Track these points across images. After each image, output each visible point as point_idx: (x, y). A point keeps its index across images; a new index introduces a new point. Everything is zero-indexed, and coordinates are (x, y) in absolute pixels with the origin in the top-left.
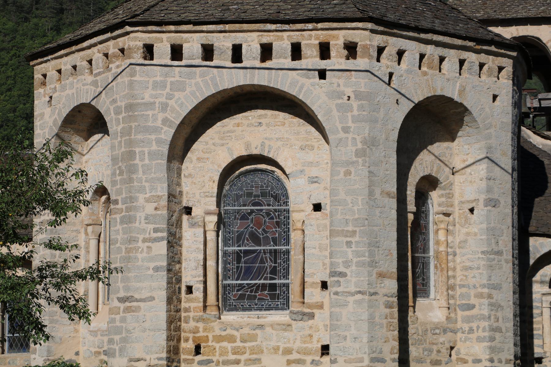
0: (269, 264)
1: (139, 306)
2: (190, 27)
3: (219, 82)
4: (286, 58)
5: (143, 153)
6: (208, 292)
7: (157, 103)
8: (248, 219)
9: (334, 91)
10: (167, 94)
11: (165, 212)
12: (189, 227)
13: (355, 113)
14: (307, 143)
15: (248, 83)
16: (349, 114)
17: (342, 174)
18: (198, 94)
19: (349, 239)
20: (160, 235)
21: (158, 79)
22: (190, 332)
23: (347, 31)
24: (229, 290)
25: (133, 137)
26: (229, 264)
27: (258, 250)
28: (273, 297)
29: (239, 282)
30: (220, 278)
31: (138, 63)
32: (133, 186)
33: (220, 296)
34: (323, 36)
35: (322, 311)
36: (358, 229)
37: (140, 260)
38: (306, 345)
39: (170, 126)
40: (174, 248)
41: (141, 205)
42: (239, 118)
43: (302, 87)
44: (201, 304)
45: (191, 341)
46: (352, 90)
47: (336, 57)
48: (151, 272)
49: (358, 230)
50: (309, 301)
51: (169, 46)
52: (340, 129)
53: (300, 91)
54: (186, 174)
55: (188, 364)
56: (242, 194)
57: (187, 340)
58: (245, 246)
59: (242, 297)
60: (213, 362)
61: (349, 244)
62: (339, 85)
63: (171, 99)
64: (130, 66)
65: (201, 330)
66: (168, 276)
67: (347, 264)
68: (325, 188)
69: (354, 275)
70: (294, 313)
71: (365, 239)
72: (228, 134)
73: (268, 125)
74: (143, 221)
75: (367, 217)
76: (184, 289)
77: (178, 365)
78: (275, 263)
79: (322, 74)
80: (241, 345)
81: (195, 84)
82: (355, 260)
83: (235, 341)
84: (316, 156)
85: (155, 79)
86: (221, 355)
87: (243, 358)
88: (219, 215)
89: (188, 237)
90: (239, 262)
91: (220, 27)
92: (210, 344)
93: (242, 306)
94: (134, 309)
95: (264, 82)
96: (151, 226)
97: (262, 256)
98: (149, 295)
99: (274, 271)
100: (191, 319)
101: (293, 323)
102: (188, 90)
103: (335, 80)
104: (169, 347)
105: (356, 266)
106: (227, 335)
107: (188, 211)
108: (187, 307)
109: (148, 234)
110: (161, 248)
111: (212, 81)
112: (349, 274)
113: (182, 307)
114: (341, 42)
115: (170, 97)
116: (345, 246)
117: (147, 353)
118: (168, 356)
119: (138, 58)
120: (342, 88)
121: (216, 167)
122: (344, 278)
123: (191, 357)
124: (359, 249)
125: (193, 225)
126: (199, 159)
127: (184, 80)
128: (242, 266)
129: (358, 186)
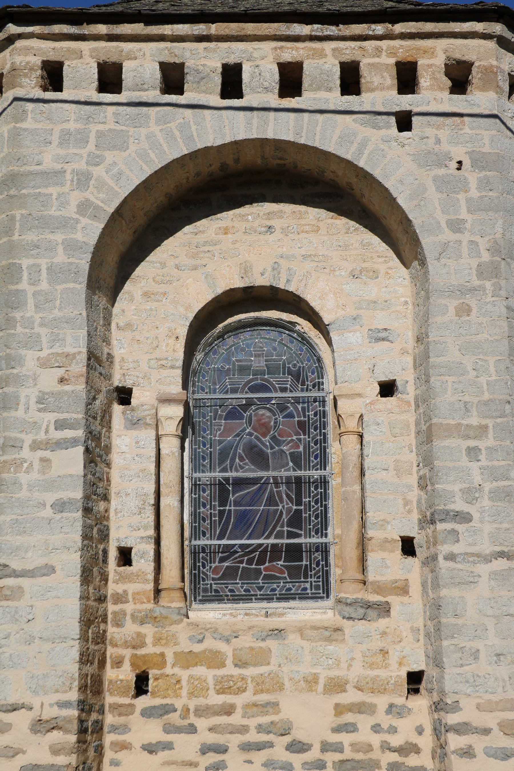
0: (286, 506)
1: (20, 587)
2: (138, 28)
3: (195, 134)
4: (330, 90)
5: (36, 269)
6: (165, 561)
7: (69, 172)
8: (241, 417)
9: (429, 152)
10: (89, 155)
11: (80, 387)
12: (126, 428)
13: (474, 193)
14: (365, 265)
15: (255, 136)
16: (461, 197)
17: (452, 312)
18: (152, 155)
19: (472, 443)
20: (69, 434)
21: (72, 126)
22: (126, 645)
23: (452, 41)
24: (203, 558)
25: (16, 237)
26: (204, 506)
27: (262, 478)
28: (295, 573)
29: (225, 542)
30: (187, 534)
31: (31, 96)
32: (15, 334)
33: (186, 571)
34: (403, 49)
35: (405, 599)
36: (490, 423)
37: (25, 487)
38: (376, 672)
39: (95, 217)
40: (96, 466)
41: (30, 373)
42: (227, 218)
43: (363, 144)
44: (151, 586)
45: (127, 666)
46: (465, 150)
47: (431, 88)
48: (48, 512)
49: (491, 425)
50: (378, 578)
51: (95, 65)
52: (444, 225)
53: (360, 152)
54: (121, 324)
55: (120, 715)
56: (229, 369)
57: (118, 663)
58: (237, 471)
59: (230, 574)
60: (176, 711)
61: (473, 453)
62: (438, 141)
63: (97, 165)
64: (15, 103)
65: (149, 640)
66: (84, 521)
67: (471, 494)
68: (404, 352)
69: (487, 519)
70: (347, 604)
71: (508, 442)
72: (206, 249)
73: (285, 231)
74: (33, 406)
75: (509, 398)
76: (113, 554)
77: (100, 718)
78: (299, 503)
79: (404, 121)
80: (236, 672)
81: (148, 137)
82: (487, 487)
83: (223, 665)
84: (384, 290)
85: (66, 126)
86: (191, 694)
87: (239, 700)
88: (186, 405)
89: (124, 448)
90: (223, 501)
91: (200, 29)
92: (168, 670)
93: (231, 591)
94: (8, 593)
95: (287, 135)
96: (51, 417)
97: (272, 490)
98: (41, 561)
99: (296, 520)
100: (128, 618)
101: (347, 624)
102: (133, 148)
103: (430, 132)
104: (83, 676)
105: (491, 499)
106: (204, 652)
107: (124, 396)
108: (120, 591)
109: (42, 433)
110: (72, 462)
111: (181, 132)
112: (476, 516)
113: (110, 592)
114: (440, 61)
115: (95, 160)
116: (465, 458)
117: (35, 692)
118: (82, 698)
119: (30, 86)
120: (445, 147)
121: (181, 309)
122: (466, 525)
123: (127, 701)
124: (496, 463)
125: (134, 424)
126: (146, 295)
127: (123, 128)
128: (230, 511)
129: (486, 335)
